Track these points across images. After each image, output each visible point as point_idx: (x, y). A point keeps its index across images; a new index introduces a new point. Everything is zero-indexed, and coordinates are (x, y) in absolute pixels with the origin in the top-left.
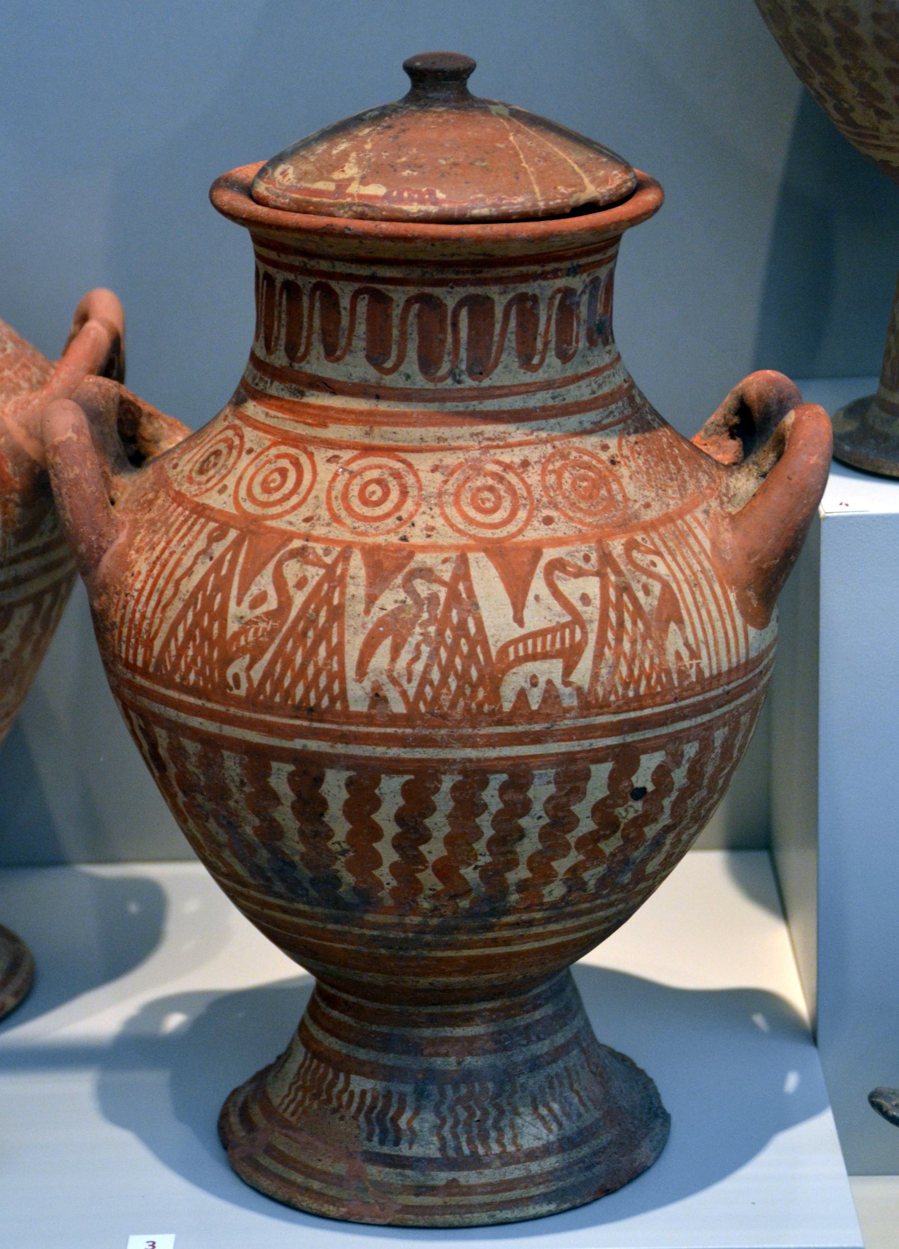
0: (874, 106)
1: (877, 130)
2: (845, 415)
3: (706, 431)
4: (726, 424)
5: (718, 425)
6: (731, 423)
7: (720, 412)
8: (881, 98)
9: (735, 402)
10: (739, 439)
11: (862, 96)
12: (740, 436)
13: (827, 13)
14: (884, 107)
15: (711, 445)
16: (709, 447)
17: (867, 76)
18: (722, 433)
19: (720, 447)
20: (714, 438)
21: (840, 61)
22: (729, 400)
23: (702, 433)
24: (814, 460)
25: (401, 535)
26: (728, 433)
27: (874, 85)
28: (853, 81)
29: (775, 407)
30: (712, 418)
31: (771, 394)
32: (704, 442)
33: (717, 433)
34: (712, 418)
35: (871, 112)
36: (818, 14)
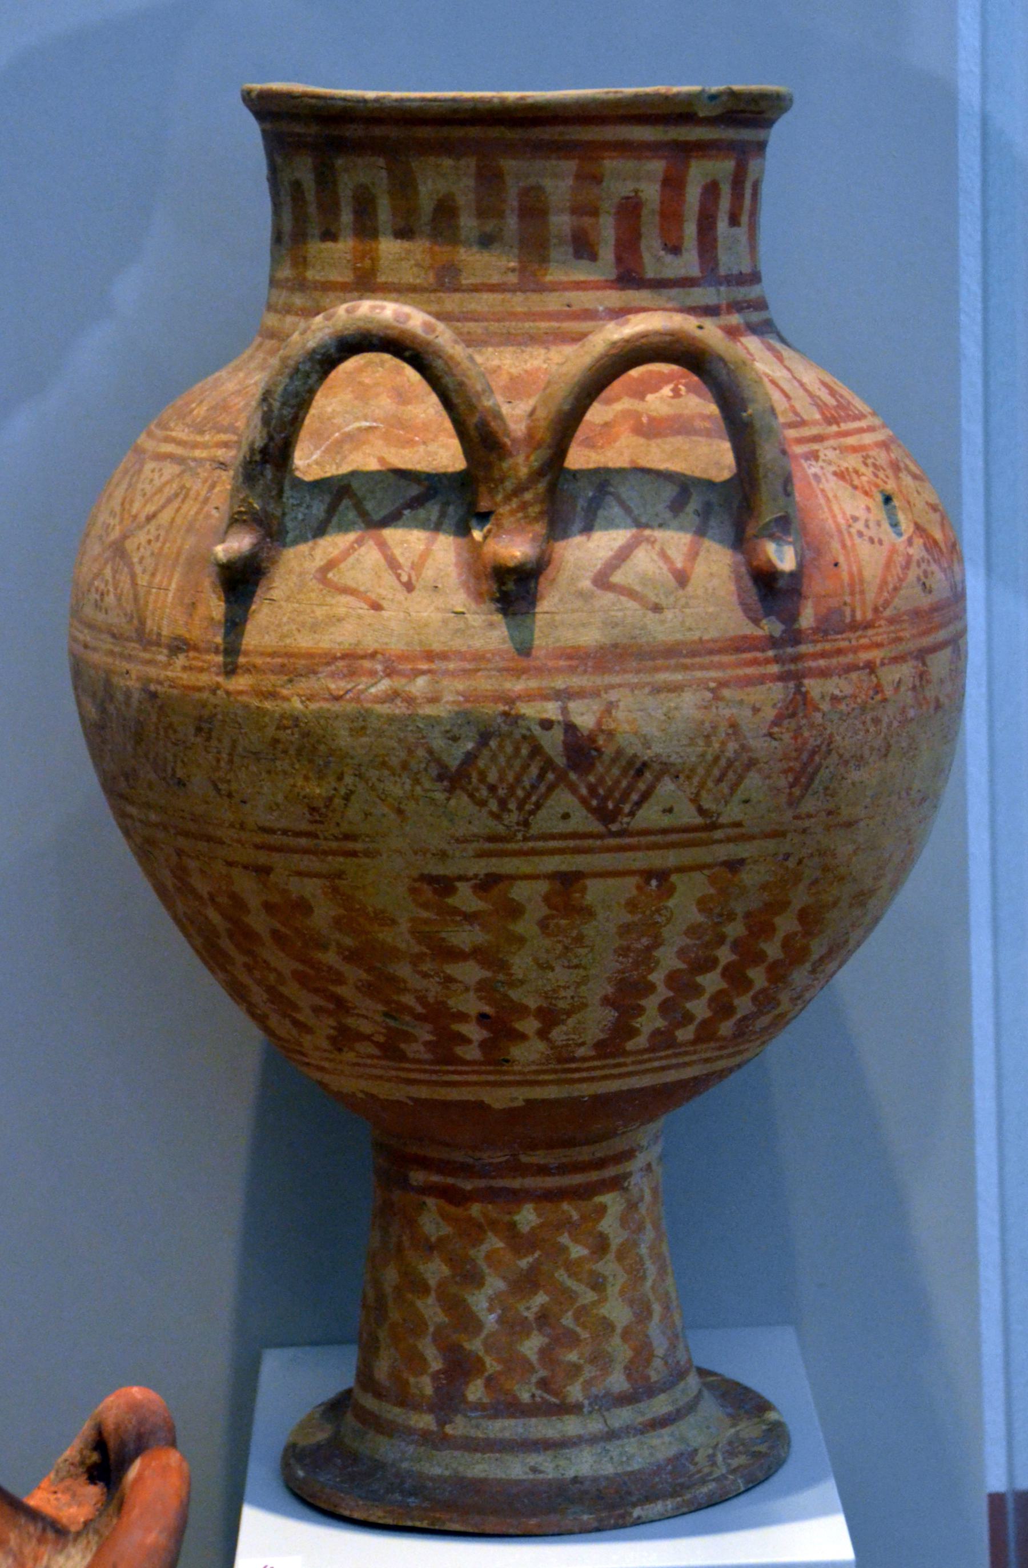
0: (289, 1016)
1: (300, 1045)
2: (324, 1413)
3: (57, 1472)
4: (82, 1463)
5: (72, 1464)
6: (89, 1462)
7: (74, 1448)
8: (295, 1007)
9: (93, 1432)
10: (101, 1484)
11: (272, 1003)
12: (101, 1480)
13: (212, 898)
14: (300, 1017)
15: (63, 1492)
16: (59, 1495)
17: (272, 977)
18: (77, 1476)
19: (74, 1495)
20: (67, 1482)
21: (240, 959)
22: (86, 1429)
23: (52, 1476)
24: (151, 1538)
25: (654, 1167)
26: (85, 1476)
27: (282, 989)
28: (259, 983)
29: (132, 1446)
30: (67, 1454)
31: (130, 1426)
32: (53, 1489)
33: (71, 1476)
34: (67, 1454)
35: (287, 1022)
36: (201, 897)
